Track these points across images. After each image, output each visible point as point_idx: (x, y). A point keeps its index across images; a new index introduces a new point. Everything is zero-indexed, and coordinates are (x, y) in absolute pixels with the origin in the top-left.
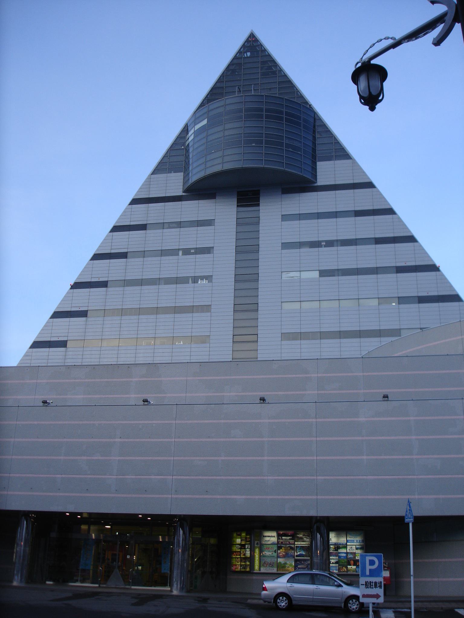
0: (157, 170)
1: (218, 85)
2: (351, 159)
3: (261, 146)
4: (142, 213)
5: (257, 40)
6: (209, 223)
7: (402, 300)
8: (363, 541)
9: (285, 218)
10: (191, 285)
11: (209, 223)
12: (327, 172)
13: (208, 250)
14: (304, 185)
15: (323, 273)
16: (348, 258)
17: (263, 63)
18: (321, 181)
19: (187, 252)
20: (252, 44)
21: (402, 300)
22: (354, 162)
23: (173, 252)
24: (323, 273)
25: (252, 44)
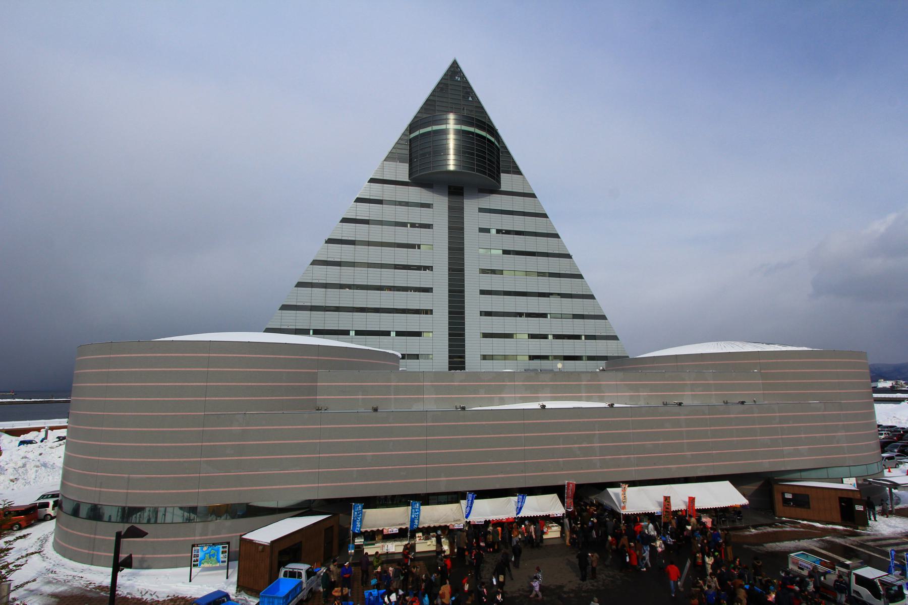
0: (388, 159)
1: (432, 98)
2: (519, 172)
3: (459, 154)
4: (377, 191)
5: (458, 67)
6: (428, 206)
7: (527, 273)
8: (133, 599)
9: (481, 210)
10: (417, 250)
11: (428, 206)
12: (507, 181)
13: (429, 226)
14: (494, 189)
15: (506, 252)
16: (520, 243)
17: (464, 88)
18: (504, 188)
19: (413, 225)
20: (454, 70)
21: (527, 273)
22: (524, 178)
23: (404, 225)
24: (506, 252)
25: (454, 70)
